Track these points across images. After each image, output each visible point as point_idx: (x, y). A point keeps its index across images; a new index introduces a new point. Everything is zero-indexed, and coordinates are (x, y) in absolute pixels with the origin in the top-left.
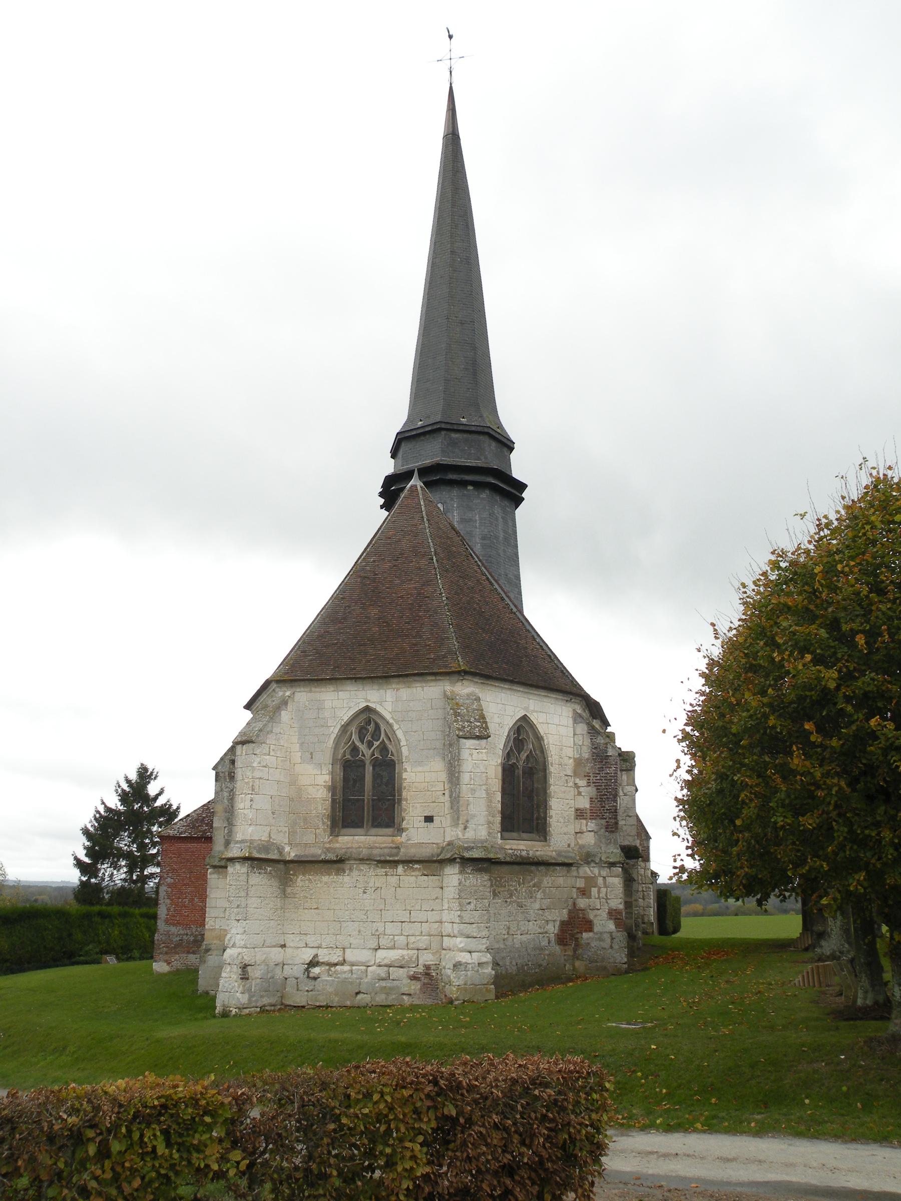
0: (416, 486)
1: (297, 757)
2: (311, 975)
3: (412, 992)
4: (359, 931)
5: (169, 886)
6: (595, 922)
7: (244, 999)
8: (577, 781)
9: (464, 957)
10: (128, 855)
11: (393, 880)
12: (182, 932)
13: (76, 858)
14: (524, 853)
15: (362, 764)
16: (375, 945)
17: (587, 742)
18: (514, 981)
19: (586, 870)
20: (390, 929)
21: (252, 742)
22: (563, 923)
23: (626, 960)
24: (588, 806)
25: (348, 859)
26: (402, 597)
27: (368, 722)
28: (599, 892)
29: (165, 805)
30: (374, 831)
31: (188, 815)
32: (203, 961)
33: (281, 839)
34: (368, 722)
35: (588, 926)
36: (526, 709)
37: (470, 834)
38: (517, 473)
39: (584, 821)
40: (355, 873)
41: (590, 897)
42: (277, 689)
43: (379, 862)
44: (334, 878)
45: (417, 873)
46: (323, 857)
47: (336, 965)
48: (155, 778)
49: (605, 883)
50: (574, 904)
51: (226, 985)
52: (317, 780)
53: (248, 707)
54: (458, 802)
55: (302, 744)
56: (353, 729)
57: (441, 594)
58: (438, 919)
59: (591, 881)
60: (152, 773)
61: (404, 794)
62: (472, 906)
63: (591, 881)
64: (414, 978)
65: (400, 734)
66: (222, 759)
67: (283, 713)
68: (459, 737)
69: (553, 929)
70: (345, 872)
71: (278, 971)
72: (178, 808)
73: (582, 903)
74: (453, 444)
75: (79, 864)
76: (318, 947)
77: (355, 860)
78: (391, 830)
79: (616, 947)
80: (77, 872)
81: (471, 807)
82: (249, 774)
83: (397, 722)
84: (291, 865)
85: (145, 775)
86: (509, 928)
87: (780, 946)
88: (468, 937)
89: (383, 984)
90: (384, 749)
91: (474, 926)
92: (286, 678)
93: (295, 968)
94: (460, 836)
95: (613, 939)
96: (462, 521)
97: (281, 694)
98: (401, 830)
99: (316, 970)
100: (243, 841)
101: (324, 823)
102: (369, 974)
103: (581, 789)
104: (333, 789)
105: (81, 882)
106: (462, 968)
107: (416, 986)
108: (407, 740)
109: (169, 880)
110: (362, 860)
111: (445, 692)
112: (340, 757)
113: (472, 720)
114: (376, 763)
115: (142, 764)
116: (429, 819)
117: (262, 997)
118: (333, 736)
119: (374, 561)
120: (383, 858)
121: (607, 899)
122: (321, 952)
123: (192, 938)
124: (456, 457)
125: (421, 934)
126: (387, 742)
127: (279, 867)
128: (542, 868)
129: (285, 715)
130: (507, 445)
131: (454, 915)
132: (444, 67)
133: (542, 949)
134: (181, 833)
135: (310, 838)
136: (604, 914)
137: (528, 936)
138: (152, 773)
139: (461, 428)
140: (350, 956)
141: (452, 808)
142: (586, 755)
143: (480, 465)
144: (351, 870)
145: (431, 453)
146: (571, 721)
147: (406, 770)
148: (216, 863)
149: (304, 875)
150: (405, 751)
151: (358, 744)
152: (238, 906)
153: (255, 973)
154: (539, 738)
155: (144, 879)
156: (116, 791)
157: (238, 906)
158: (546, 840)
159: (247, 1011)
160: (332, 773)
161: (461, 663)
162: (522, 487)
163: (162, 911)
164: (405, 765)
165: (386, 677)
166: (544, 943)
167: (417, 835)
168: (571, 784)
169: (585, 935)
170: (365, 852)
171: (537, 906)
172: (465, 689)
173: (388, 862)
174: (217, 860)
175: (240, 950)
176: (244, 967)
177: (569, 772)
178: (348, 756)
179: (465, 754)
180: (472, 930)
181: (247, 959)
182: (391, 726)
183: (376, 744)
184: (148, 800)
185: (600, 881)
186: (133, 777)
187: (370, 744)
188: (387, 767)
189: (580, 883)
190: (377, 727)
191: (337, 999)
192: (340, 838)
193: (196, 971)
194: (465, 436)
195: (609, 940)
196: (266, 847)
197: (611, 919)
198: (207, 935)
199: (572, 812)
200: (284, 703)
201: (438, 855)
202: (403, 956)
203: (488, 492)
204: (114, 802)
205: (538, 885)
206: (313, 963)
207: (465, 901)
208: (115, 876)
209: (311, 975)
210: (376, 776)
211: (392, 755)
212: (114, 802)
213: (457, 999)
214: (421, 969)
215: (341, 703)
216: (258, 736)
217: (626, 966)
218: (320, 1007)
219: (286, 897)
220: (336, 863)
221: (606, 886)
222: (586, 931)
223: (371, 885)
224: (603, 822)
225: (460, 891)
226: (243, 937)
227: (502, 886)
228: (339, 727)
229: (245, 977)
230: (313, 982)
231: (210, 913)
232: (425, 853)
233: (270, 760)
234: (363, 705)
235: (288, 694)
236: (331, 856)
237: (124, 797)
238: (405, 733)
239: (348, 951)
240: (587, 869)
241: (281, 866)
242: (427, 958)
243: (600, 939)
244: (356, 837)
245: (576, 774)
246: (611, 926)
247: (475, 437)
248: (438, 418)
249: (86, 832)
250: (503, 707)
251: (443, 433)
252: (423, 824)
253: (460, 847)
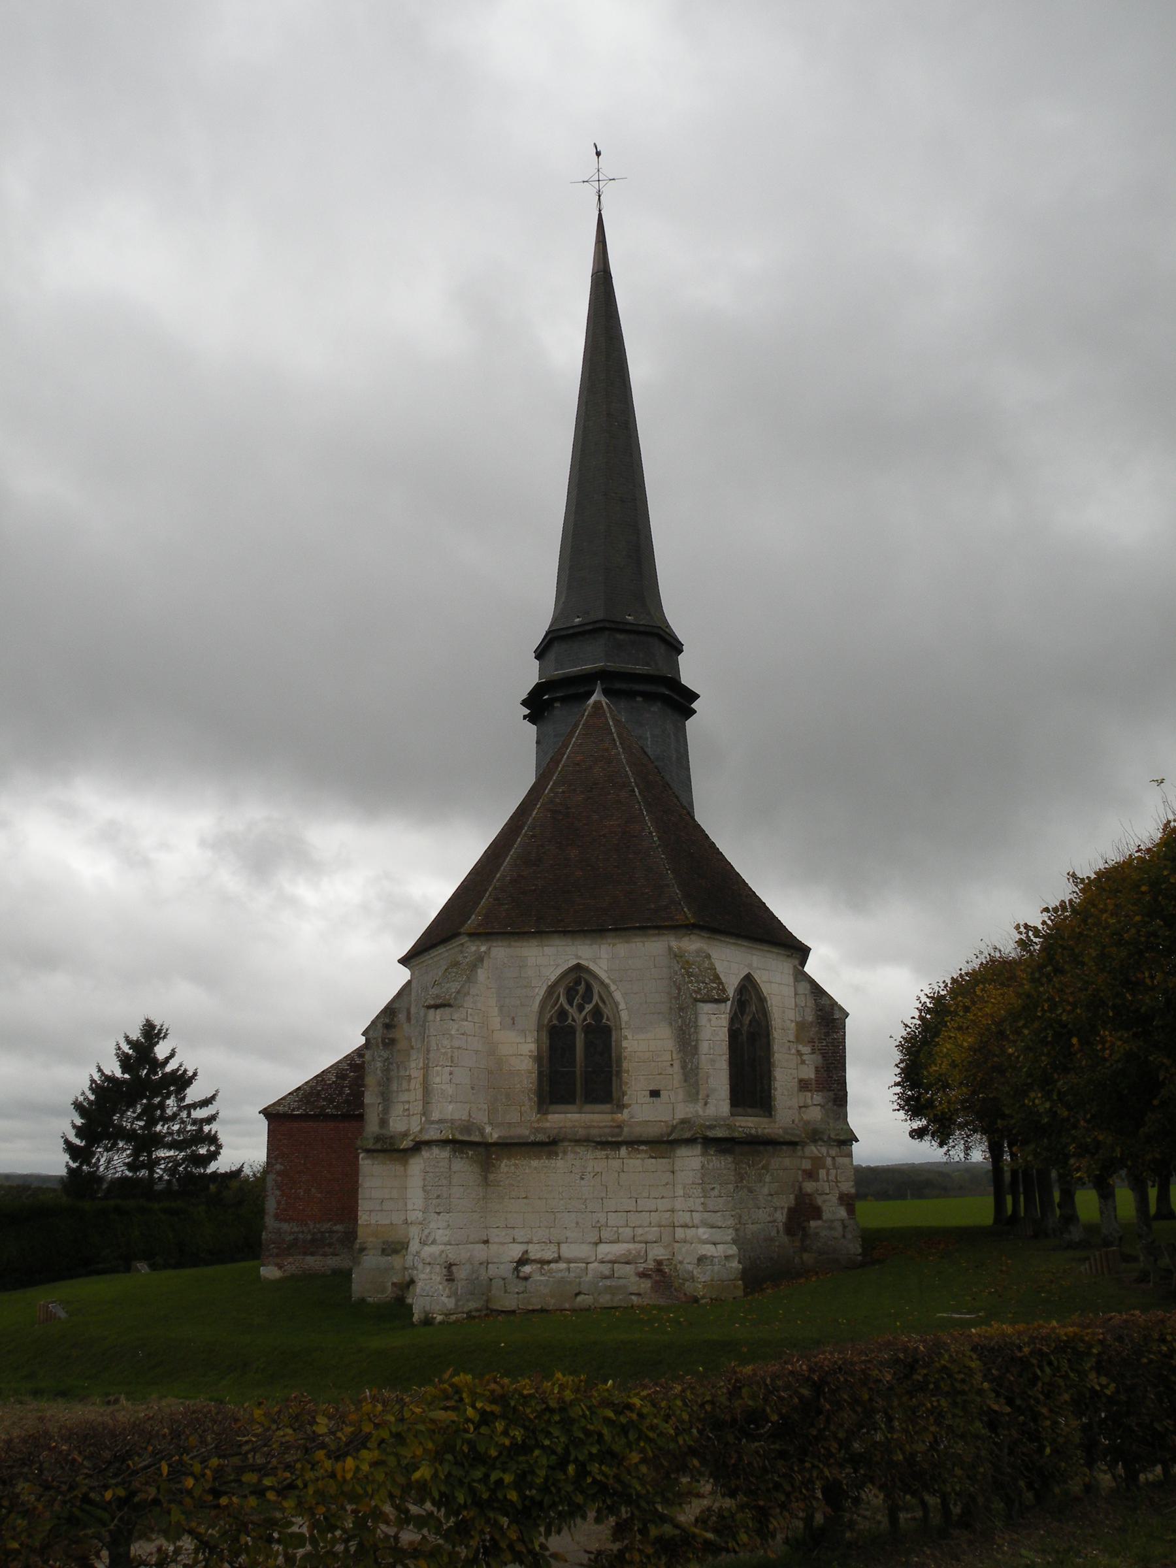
0: (600, 702)
1: (496, 1022)
2: (521, 1274)
3: (642, 1291)
4: (577, 1223)
5: (279, 1173)
6: (824, 1208)
7: (450, 1303)
8: (800, 1047)
9: (708, 1250)
10: (130, 1136)
11: (616, 1164)
12: (296, 1229)
13: (67, 1142)
14: (753, 1131)
15: (571, 1031)
16: (596, 1239)
17: (811, 1003)
18: (760, 1274)
19: (813, 1150)
20: (613, 1219)
21: (450, 1006)
22: (790, 1209)
24: (813, 1076)
25: (562, 1140)
26: (604, 836)
27: (578, 982)
28: (828, 1174)
29: (178, 1070)
30: (588, 1107)
31: (299, 1088)
32: (356, 1261)
33: (481, 1118)
34: (578, 982)
35: (817, 1213)
36: (750, 966)
37: (711, 1111)
38: (688, 679)
39: (809, 1094)
40: (570, 1156)
41: (817, 1180)
42: (469, 944)
43: (599, 1143)
44: (544, 1162)
45: (643, 1155)
46: (532, 1138)
47: (549, 1262)
48: (164, 1037)
49: (834, 1164)
50: (800, 1189)
51: (427, 1288)
52: (521, 1050)
53: (404, 961)
54: (697, 1075)
55: (501, 1008)
56: (562, 990)
57: (651, 833)
58: (669, 1208)
59: (818, 1162)
60: (160, 1030)
61: (625, 1065)
62: (716, 1192)
63: (818, 1162)
64: (643, 1275)
65: (618, 996)
66: (373, 1022)
67: (479, 971)
68: (696, 1000)
69: (781, 1217)
70: (557, 1155)
71: (482, 1271)
72: (195, 1074)
73: (809, 1187)
75: (70, 1148)
76: (527, 1243)
77: (571, 1141)
78: (609, 1106)
79: (849, 1236)
80: (67, 1157)
81: (711, 1080)
82: (446, 1042)
83: (614, 981)
84: (494, 1149)
85: (152, 1033)
87: (967, 1236)
88: (712, 1227)
89: (608, 1282)
90: (597, 1013)
91: (719, 1214)
92: (481, 930)
93: (502, 1266)
94: (701, 1113)
97: (473, 949)
98: (621, 1107)
99: (527, 1269)
100: (440, 1121)
101: (530, 1099)
102: (590, 1272)
103: (805, 1057)
104: (538, 1059)
105: (71, 1171)
106: (708, 1262)
107: (646, 1285)
108: (627, 1004)
109: (278, 1167)
110: (578, 1142)
111: (670, 948)
112: (546, 1022)
113: (707, 980)
114: (588, 1029)
115: (147, 1020)
116: (655, 1094)
117: (468, 1301)
118: (539, 999)
119: (563, 792)
120: (604, 1139)
121: (837, 1182)
122: (531, 1247)
123: (309, 1237)
124: (609, 661)
125: (650, 1225)
126: (601, 1004)
127: (482, 1151)
128: (770, 1148)
129: (481, 974)
130: (675, 647)
131: (696, 1203)
132: (590, 191)
133: (772, 1240)
134: (293, 1110)
135: (513, 1117)
136: (834, 1199)
138: (160, 1030)
139: (628, 627)
140: (567, 1251)
141: (685, 1081)
142: (810, 1018)
143: (651, 672)
144: (565, 1153)
145: (589, 658)
146: (791, 980)
147: (626, 1038)
148: (370, 1146)
149: (509, 1159)
150: (624, 1016)
151: (567, 1007)
152: (438, 1197)
153: (461, 1273)
154: (762, 1000)
155: (152, 1164)
156: (117, 1055)
157: (438, 1197)
158: (770, 1116)
159: (453, 1317)
160: (538, 1041)
161: (688, 914)
162: (694, 696)
163: (271, 1205)
164: (625, 1032)
165: (601, 931)
166: (774, 1233)
167: (642, 1112)
168: (793, 1051)
169: (813, 1224)
170: (582, 1132)
171: (766, 1190)
172: (692, 945)
173: (609, 1144)
174: (372, 1141)
175: (442, 1247)
176: (449, 1266)
177: (792, 1038)
178: (555, 1022)
179: (703, 1020)
180: (717, 1219)
181: (452, 1257)
182: (606, 986)
183: (588, 1007)
184: (157, 1065)
185: (829, 1161)
186: (136, 1035)
187: (581, 1008)
188: (602, 1035)
189: (807, 1165)
190: (589, 988)
191: (553, 1301)
192: (550, 1117)
193: (349, 1273)
195: (840, 1229)
196: (467, 1128)
197: (841, 1204)
198: (361, 1232)
199: (795, 1083)
200: (481, 959)
201: (669, 1135)
202: (629, 1250)
203: (659, 704)
204: (114, 1069)
206: (522, 1261)
207: (709, 1187)
208: (114, 1162)
209: (521, 1274)
210: (588, 1045)
211: (608, 1019)
212: (114, 1069)
213: (703, 1298)
214: (651, 1265)
215: (546, 961)
216: (455, 998)
217: (860, 1258)
218: (534, 1311)
219: (488, 1185)
220: (548, 1146)
221: (835, 1167)
222: (813, 1219)
223: (589, 1169)
224: (831, 1094)
225: (703, 1175)
226: (447, 1232)
228: (545, 988)
229: (450, 1279)
230: (524, 1283)
231: (364, 1206)
232: (653, 1132)
233: (467, 1026)
234: (574, 962)
235: (483, 949)
236: (540, 1137)
237: (125, 1062)
238: (625, 995)
239: (564, 1247)
240: (813, 1148)
241: (481, 1150)
242: (658, 1252)
243: (831, 1228)
244: (569, 1115)
245: (798, 1039)
248: (600, 615)
249: (78, 1106)
250: (731, 962)
251: (607, 633)
252: (648, 1099)
253: (702, 1125)
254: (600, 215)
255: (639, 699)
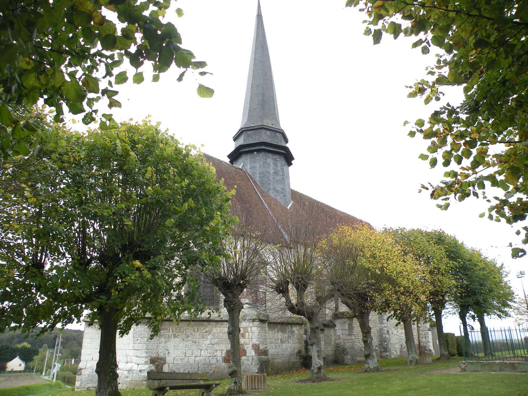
6: (247, 351)
23: (257, 371)
62: (139, 341)
74: (249, 136)
79: (253, 364)
86: (185, 353)
95: (253, 360)
96: (251, 168)
136: (250, 346)
137: (201, 358)
145: (241, 141)
171: (208, 342)
194: (254, 131)
205: (209, 332)
221: (252, 332)
227: (180, 332)
243: (248, 360)
246: (253, 353)
247: (259, 130)
251: (244, 132)
254: (259, 17)
255: (255, 153)
